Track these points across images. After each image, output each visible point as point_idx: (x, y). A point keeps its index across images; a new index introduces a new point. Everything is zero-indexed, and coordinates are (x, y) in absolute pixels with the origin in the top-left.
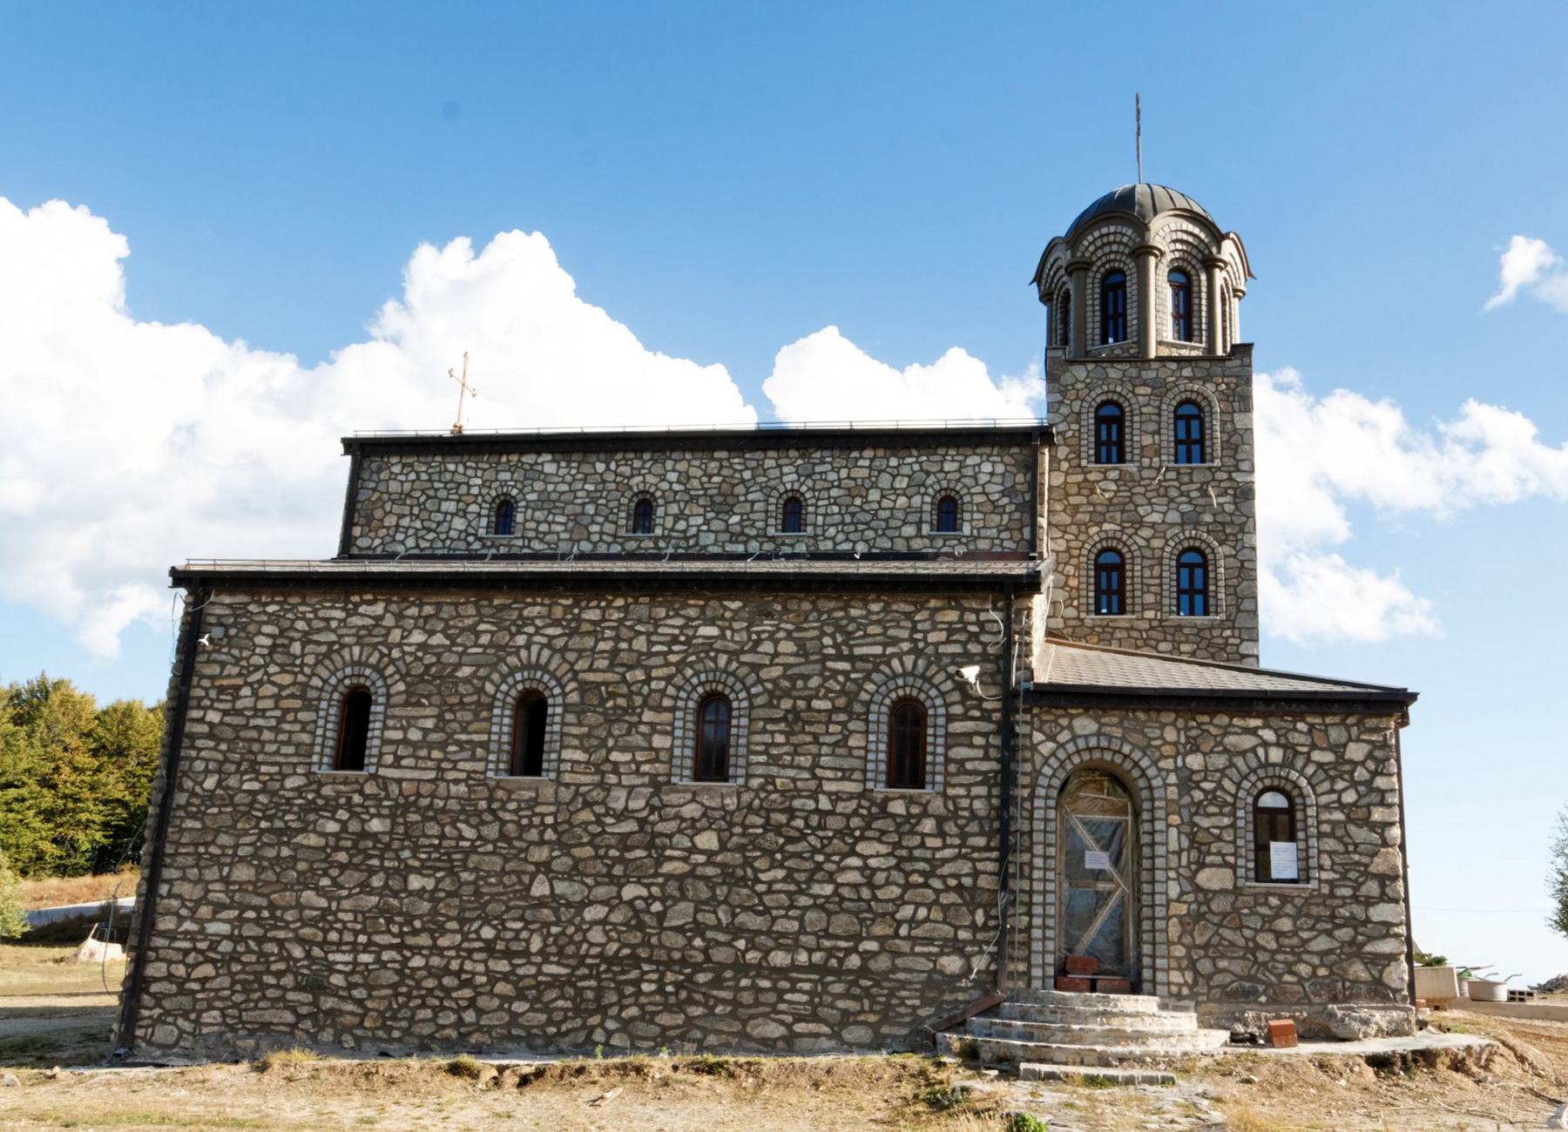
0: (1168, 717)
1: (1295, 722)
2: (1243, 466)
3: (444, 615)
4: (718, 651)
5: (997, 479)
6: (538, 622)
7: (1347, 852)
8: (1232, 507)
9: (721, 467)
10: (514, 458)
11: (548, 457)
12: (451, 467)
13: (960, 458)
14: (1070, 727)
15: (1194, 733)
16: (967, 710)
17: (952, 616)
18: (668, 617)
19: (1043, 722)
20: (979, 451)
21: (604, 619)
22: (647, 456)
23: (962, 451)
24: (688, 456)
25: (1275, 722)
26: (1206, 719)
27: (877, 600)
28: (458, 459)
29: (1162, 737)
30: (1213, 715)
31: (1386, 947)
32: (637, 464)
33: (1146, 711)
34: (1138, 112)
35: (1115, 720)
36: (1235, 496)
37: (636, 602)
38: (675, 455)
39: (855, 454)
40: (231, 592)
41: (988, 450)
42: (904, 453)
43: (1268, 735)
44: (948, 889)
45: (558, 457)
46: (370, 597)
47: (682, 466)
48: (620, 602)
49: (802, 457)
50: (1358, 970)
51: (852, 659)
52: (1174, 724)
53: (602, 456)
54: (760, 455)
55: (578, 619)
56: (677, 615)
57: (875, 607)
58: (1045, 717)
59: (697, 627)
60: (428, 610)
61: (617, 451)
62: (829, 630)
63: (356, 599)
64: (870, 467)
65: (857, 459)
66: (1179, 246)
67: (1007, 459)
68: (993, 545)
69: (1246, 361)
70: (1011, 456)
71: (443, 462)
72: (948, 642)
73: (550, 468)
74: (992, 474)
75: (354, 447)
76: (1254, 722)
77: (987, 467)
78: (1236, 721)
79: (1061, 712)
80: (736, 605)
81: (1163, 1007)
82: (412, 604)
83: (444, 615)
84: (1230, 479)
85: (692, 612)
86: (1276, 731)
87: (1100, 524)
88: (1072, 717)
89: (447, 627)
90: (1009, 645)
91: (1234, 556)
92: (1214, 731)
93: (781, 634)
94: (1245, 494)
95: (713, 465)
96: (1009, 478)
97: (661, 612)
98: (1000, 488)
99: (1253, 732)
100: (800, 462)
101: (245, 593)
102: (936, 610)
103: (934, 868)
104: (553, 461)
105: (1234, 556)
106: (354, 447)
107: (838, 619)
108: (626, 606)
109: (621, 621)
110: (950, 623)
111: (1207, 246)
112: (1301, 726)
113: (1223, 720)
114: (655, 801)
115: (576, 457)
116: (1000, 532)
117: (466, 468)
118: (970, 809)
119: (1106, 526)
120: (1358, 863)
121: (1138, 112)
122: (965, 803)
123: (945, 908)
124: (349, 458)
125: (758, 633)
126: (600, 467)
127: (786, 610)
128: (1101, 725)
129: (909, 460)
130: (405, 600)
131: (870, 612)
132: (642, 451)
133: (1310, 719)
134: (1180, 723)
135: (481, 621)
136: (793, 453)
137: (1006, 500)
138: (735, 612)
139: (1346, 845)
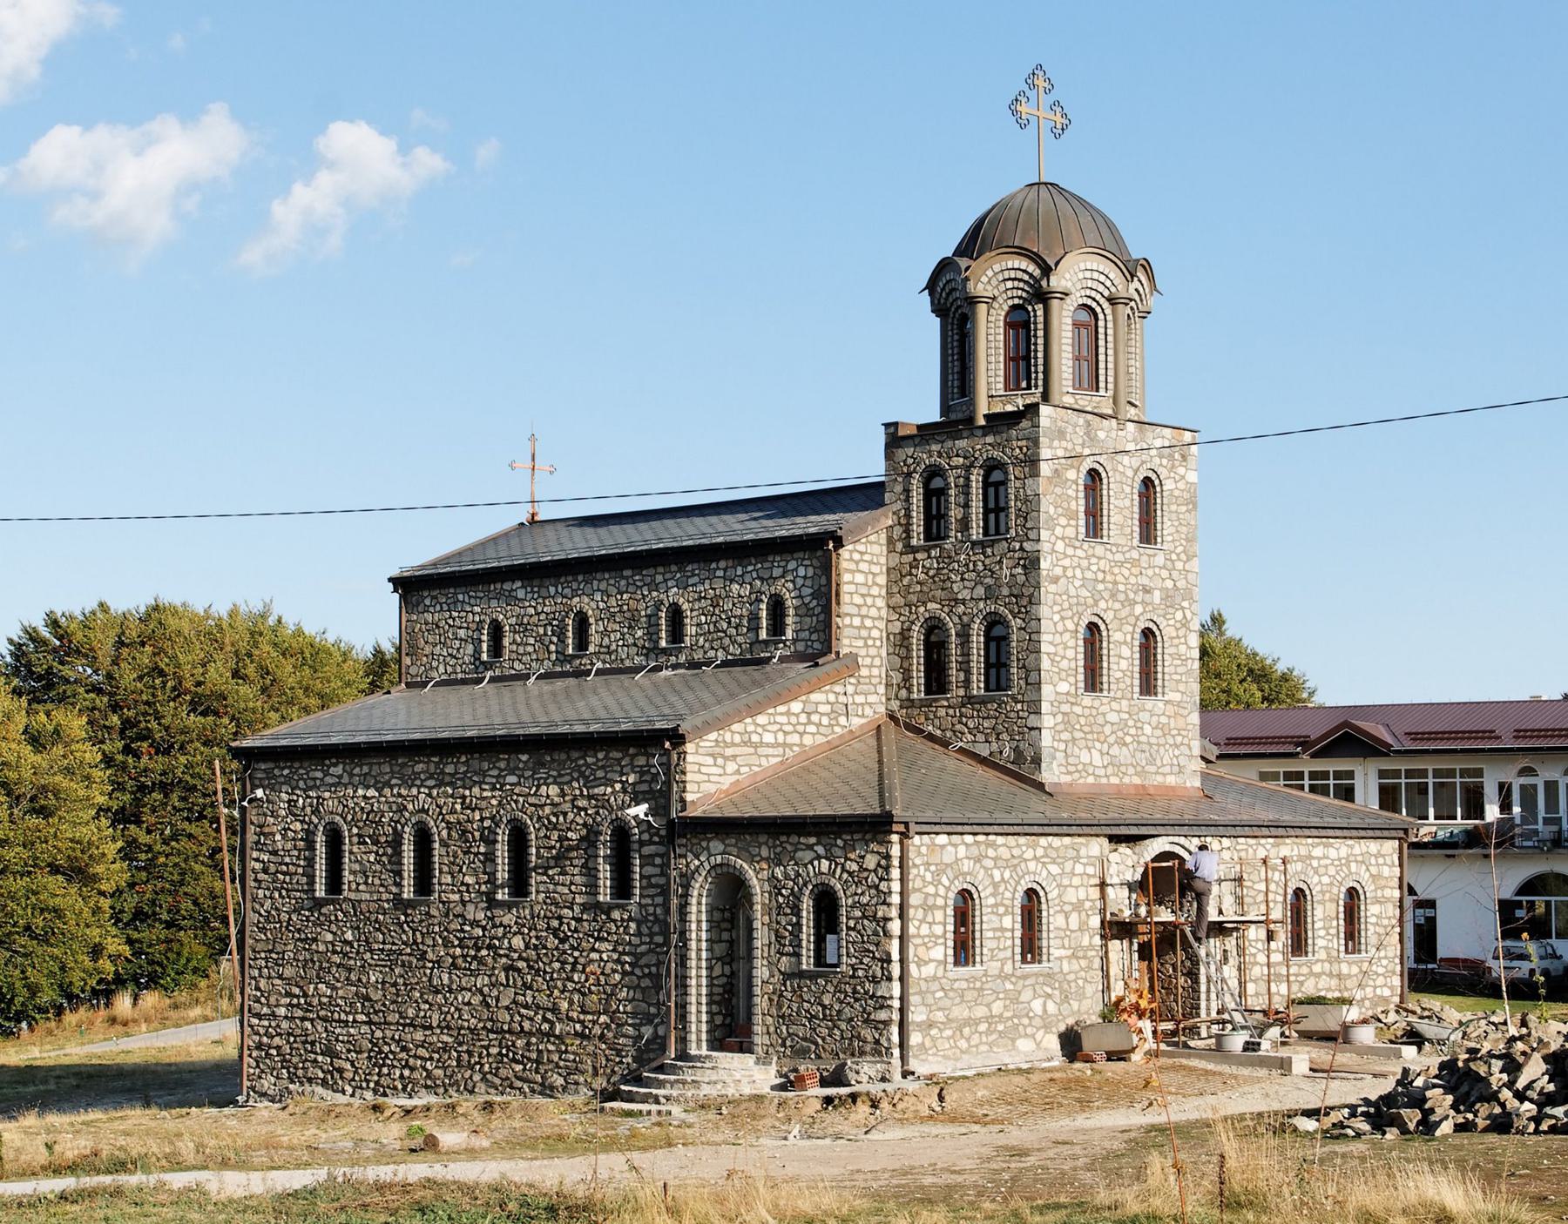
0: (763, 838)
1: (835, 839)
2: (1032, 535)
3: (374, 773)
4: (518, 795)
5: (808, 582)
6: (422, 776)
7: (863, 942)
8: (1023, 578)
9: (628, 584)
10: (498, 586)
11: (519, 584)
12: (460, 597)
13: (783, 564)
14: (708, 849)
15: (779, 850)
16: (651, 837)
17: (641, 761)
18: (489, 769)
19: (693, 845)
20: (795, 556)
21: (456, 773)
22: (580, 578)
23: (784, 557)
24: (607, 576)
25: (825, 840)
26: (784, 838)
27: (602, 750)
28: (464, 589)
29: (759, 855)
30: (788, 835)
31: (882, 1015)
32: (575, 586)
33: (750, 834)
34: (533, 460)
35: (733, 841)
36: (1024, 567)
37: (472, 758)
38: (599, 576)
39: (714, 565)
40: (265, 761)
41: (801, 555)
42: (745, 562)
43: (820, 850)
44: (644, 976)
45: (526, 583)
46: (334, 761)
47: (603, 586)
48: (463, 759)
49: (680, 570)
50: (867, 1034)
51: (590, 797)
52: (766, 844)
53: (553, 581)
54: (651, 571)
55: (442, 772)
56: (495, 767)
57: (601, 755)
58: (695, 841)
59: (505, 776)
60: (366, 769)
61: (560, 576)
62: (575, 775)
63: (327, 762)
64: (724, 578)
65: (715, 570)
66: (1009, 284)
67: (815, 562)
68: (807, 646)
69: (1036, 420)
70: (817, 558)
71: (455, 594)
72: (641, 782)
73: (521, 594)
74: (805, 577)
75: (402, 584)
76: (813, 840)
77: (801, 572)
78: (802, 840)
79: (702, 836)
80: (524, 758)
81: (757, 1063)
82: (357, 765)
83: (374, 773)
84: (1022, 549)
85: (502, 765)
86: (824, 846)
87: (924, 603)
88: (709, 840)
89: (377, 782)
90: (668, 783)
91: (1024, 629)
92: (789, 848)
93: (551, 780)
94: (1031, 564)
95: (623, 582)
96: (816, 582)
97: (485, 765)
98: (810, 591)
99: (810, 847)
100: (678, 575)
101: (271, 760)
102: (633, 757)
103: (638, 959)
104: (522, 587)
105: (1024, 629)
106: (402, 584)
107: (580, 766)
108: (467, 761)
109: (465, 773)
110: (641, 767)
111: (1037, 281)
112: (839, 842)
113: (794, 839)
114: (489, 914)
115: (536, 582)
116: (811, 633)
117: (470, 597)
118: (654, 914)
119: (930, 606)
120: (869, 951)
121: (533, 460)
122: (651, 910)
123: (644, 990)
124: (396, 596)
125: (539, 779)
126: (552, 590)
127: (553, 760)
128: (726, 846)
129: (750, 568)
130: (353, 762)
131: (598, 760)
132: (578, 574)
133: (844, 837)
134: (770, 843)
135: (393, 777)
136: (674, 568)
137: (815, 602)
138: (525, 762)
139: (862, 936)
